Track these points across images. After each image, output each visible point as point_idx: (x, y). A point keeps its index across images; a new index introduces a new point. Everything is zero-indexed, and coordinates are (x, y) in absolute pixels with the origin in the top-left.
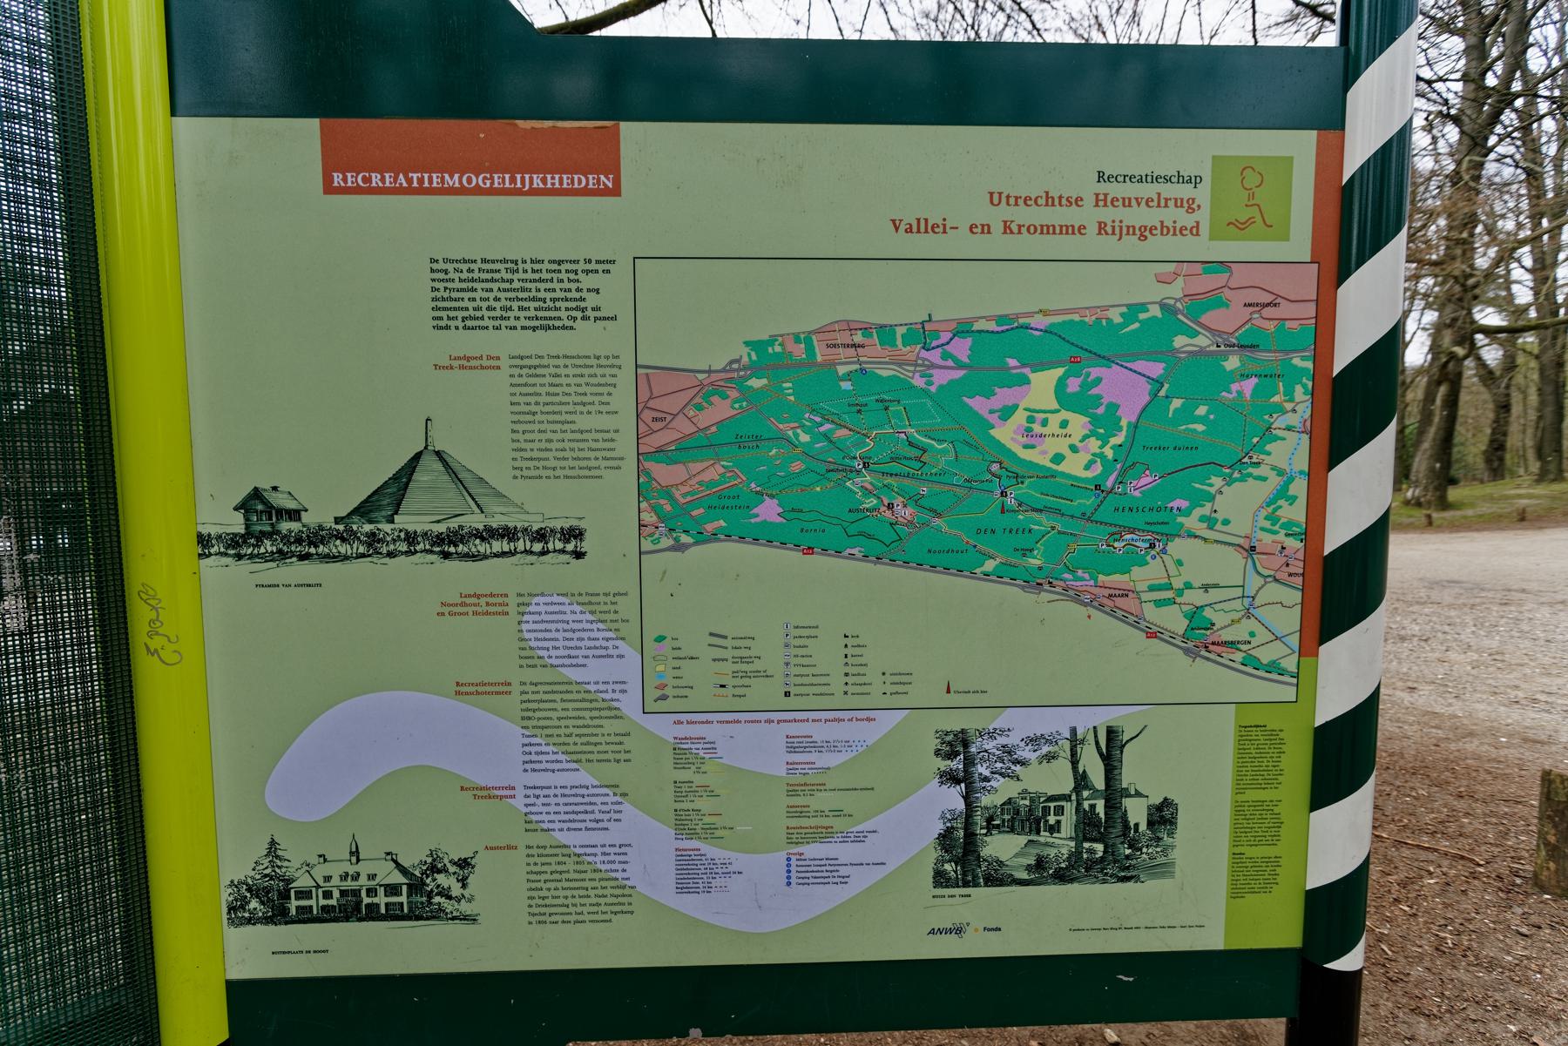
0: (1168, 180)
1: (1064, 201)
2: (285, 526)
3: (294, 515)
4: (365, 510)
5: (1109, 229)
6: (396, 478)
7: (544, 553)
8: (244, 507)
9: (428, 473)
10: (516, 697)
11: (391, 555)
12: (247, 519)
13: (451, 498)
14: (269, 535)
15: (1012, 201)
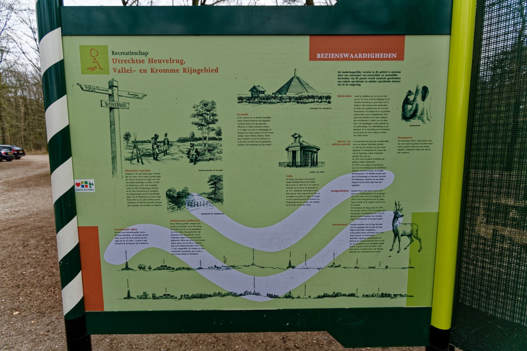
0: (136, 54)
1: (138, 61)
2: (261, 95)
3: (263, 92)
4: (279, 91)
5: (187, 71)
6: (287, 83)
7: (321, 102)
8: (252, 90)
9: (295, 82)
10: (352, 146)
11: (285, 102)
12: (252, 93)
13: (300, 88)
14: (257, 97)
15: (120, 61)
